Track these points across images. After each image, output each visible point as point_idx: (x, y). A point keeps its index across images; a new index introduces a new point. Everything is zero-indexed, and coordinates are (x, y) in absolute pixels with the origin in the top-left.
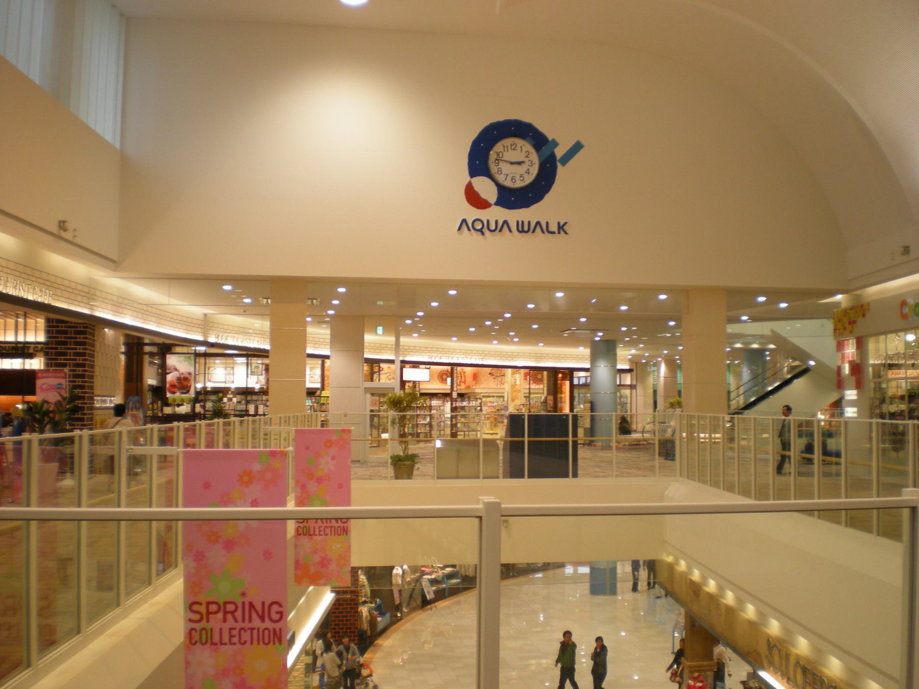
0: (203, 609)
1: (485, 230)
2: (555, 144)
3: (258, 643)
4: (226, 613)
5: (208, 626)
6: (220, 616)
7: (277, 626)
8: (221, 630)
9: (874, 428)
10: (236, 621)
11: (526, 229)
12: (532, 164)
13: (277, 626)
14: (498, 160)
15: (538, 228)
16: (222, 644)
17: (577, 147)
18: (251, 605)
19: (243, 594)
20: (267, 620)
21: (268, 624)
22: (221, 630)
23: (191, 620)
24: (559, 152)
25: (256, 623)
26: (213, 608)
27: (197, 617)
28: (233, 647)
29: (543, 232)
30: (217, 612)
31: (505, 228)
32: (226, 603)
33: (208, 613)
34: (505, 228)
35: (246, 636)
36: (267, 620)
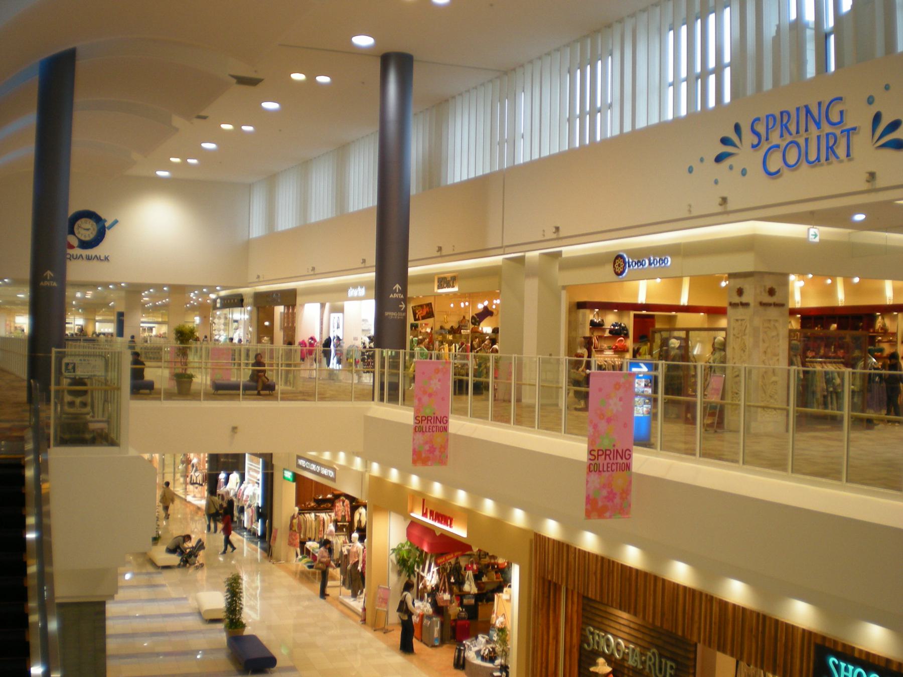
0: (595, 453)
1: (71, 258)
2: (105, 221)
3: (620, 470)
4: (606, 455)
5: (422, 425)
6: (603, 457)
7: (628, 461)
8: (603, 464)
9: (664, 365)
10: (431, 423)
11: (90, 258)
12: (94, 230)
13: (628, 461)
14: (79, 227)
15: (96, 258)
16: (603, 471)
18: (617, 451)
19: (434, 414)
20: (624, 458)
21: (442, 424)
22: (603, 464)
23: (590, 459)
24: (107, 225)
25: (438, 424)
26: (600, 453)
27: (593, 457)
28: (609, 473)
29: (98, 259)
30: (424, 420)
31: (81, 258)
32: (606, 450)
33: (598, 455)
34: (81, 258)
35: (614, 467)
36: (624, 458)
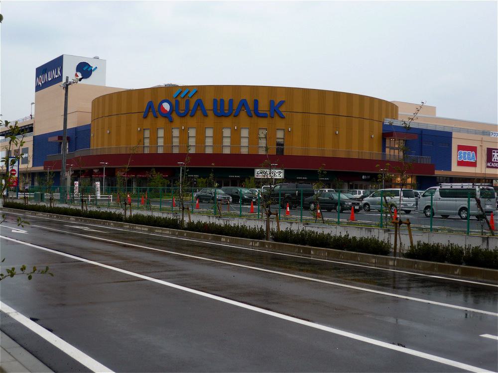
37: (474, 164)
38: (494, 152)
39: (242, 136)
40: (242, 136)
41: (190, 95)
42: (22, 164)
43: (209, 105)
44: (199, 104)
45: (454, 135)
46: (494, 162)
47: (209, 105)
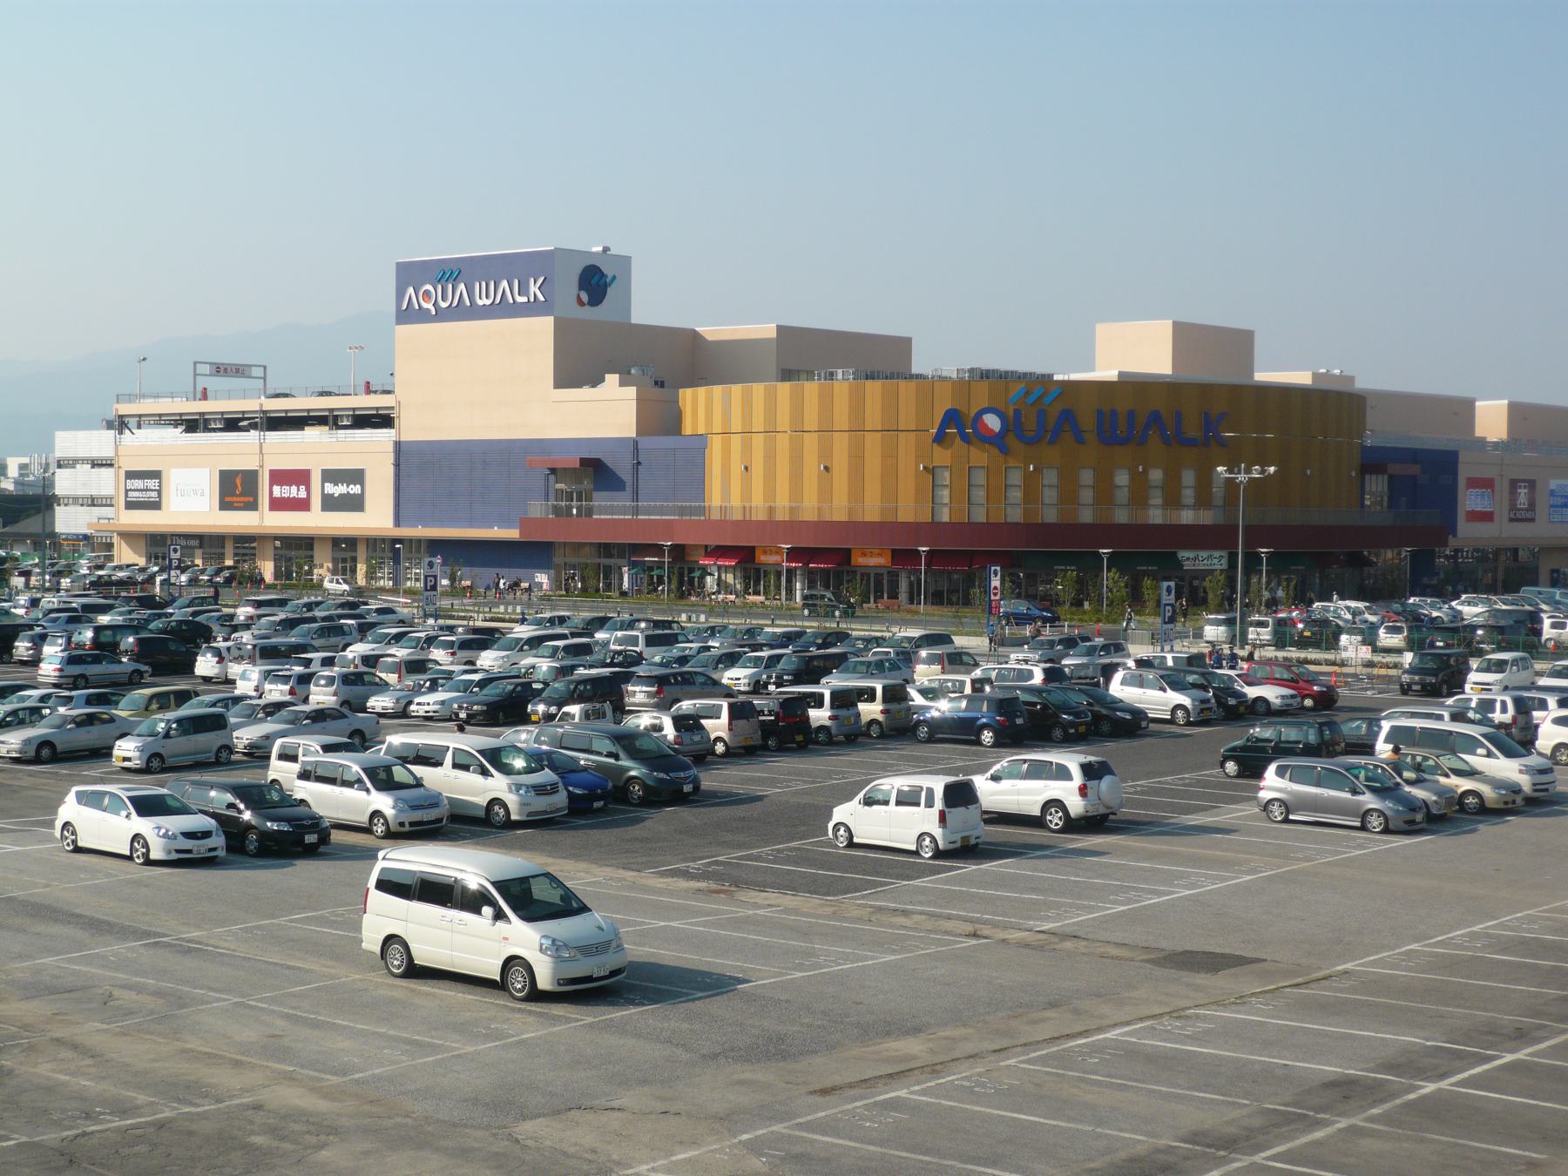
17: (614, 278)
37: (302, 505)
38: (1520, 487)
39: (1184, 485)
40: (1184, 485)
41: (1047, 400)
42: (1173, 657)
43: (1087, 422)
44: (1068, 417)
45: (1461, 458)
46: (1519, 510)
47: (1087, 422)
